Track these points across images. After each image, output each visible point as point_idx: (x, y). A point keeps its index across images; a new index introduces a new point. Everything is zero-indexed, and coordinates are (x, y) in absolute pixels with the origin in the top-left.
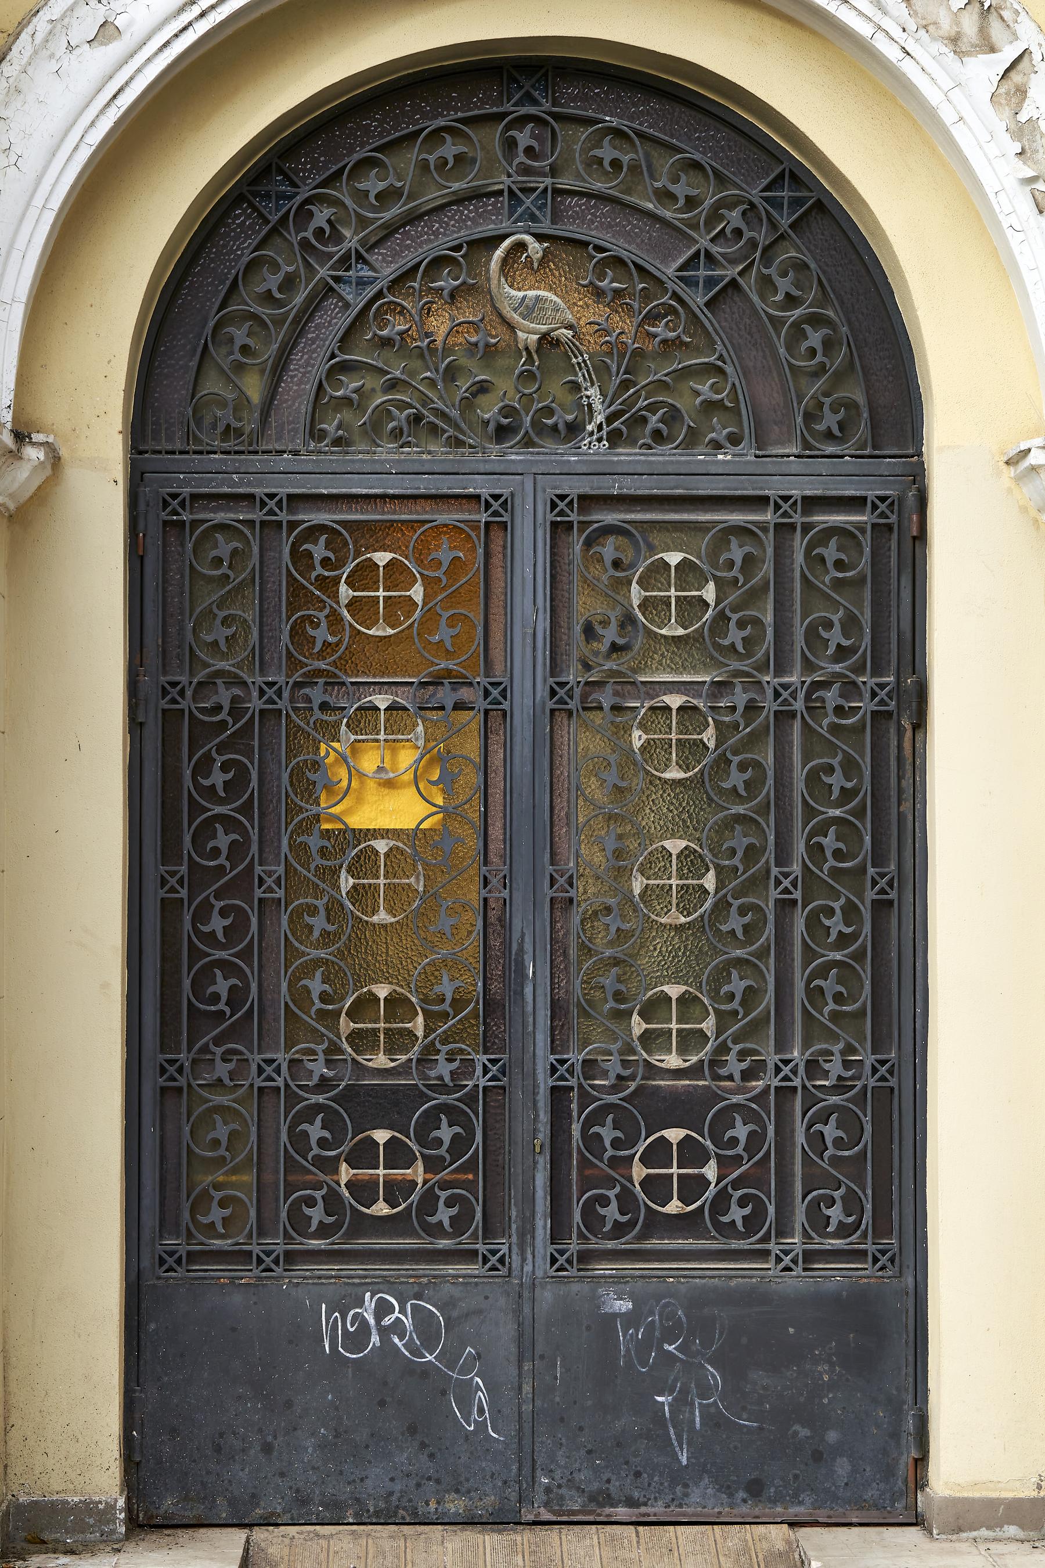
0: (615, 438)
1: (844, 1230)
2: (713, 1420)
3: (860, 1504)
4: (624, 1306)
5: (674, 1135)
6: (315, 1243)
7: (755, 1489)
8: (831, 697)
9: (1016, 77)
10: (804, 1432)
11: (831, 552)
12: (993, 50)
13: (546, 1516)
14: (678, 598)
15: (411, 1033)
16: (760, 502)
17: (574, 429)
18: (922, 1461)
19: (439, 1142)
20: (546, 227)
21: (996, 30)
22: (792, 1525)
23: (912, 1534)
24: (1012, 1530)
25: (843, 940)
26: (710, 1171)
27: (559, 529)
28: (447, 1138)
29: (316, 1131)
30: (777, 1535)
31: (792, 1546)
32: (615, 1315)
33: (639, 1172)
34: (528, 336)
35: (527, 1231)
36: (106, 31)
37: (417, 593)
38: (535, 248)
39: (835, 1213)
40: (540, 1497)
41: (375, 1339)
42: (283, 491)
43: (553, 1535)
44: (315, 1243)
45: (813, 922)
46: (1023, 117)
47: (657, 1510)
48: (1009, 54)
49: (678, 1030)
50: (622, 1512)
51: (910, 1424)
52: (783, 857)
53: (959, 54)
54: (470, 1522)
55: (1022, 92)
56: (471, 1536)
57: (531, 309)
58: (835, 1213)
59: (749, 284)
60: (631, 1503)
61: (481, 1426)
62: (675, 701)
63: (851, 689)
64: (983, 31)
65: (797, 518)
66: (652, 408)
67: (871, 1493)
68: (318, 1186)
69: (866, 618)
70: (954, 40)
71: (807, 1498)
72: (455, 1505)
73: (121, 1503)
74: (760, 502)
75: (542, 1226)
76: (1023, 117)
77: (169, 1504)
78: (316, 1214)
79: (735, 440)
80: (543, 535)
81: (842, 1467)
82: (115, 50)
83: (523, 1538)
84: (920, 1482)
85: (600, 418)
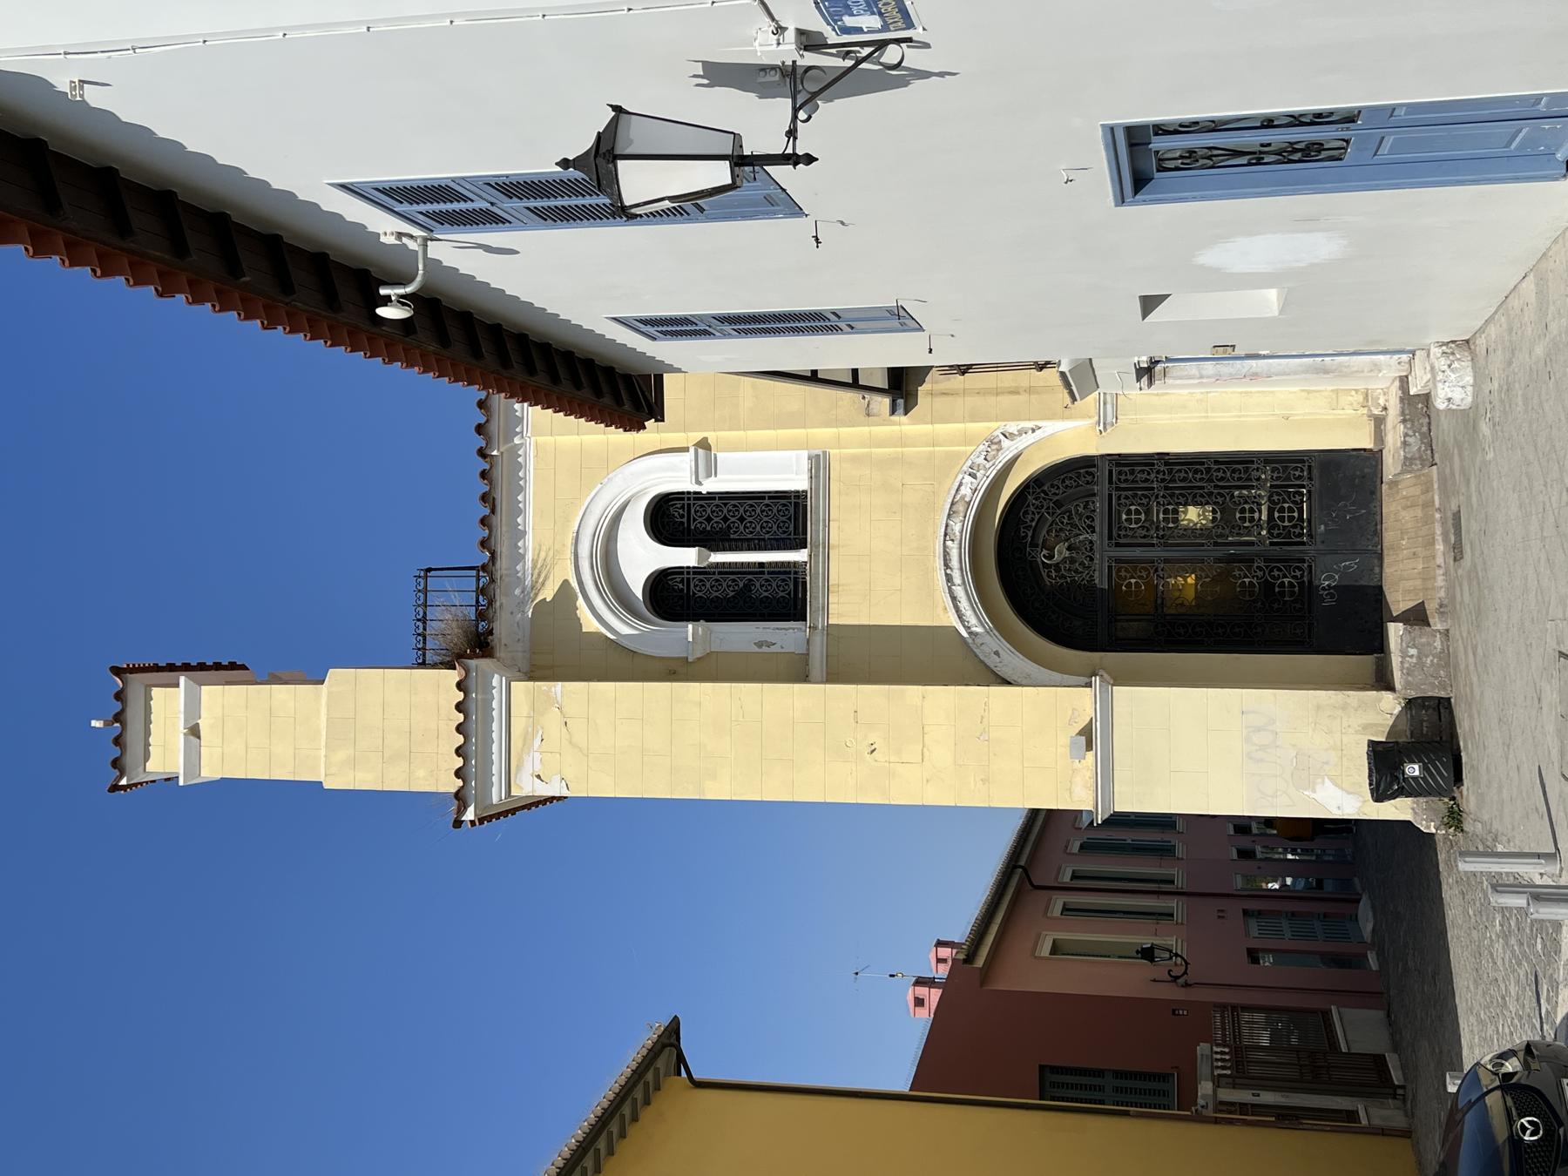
0: (1093, 532)
1: (1302, 471)
2: (1353, 504)
3: (1377, 466)
4: (1322, 527)
5: (1124, 517)
6: (1306, 606)
7: (1373, 493)
8: (1161, 476)
9: (1007, 435)
10: (1357, 480)
11: (1123, 477)
12: (1000, 441)
13: (1380, 547)
14: (1288, 516)
15: (1249, 582)
16: (1110, 496)
17: (1091, 542)
18: (1365, 450)
19: (1278, 575)
20: (1039, 549)
21: (996, 440)
22: (1382, 483)
23: (1384, 451)
24: (1382, 427)
25: (1224, 472)
26: (1286, 505)
27: (1118, 545)
28: (1278, 573)
29: (1276, 606)
30: (1384, 487)
31: (1387, 483)
32: (1325, 529)
33: (1286, 524)
34: (1067, 554)
35: (1301, 552)
36: (997, 653)
37: (1133, 581)
38: (1045, 552)
39: (1297, 473)
40: (1375, 548)
41: (1332, 591)
42: (1107, 486)
43: (1384, 545)
44: (1306, 606)
45: (1222, 479)
46: (1017, 433)
47: (1378, 518)
48: (1002, 437)
49: (1288, 512)
50: (1379, 527)
51: (1354, 453)
52: (1203, 488)
53: (1001, 449)
54: (1381, 566)
55: (1010, 434)
56: (1385, 565)
57: (1060, 553)
58: (1297, 473)
59: (1055, 499)
60: (1376, 525)
61: (1356, 564)
62: (1161, 516)
63: (1158, 472)
64: (996, 444)
65: (1114, 486)
66: (1085, 522)
67: (1374, 463)
68: (1290, 606)
69: (1140, 468)
70: (998, 450)
71: (1375, 479)
72: (1377, 570)
73: (1375, 655)
74: (1110, 496)
75: (1301, 548)
76: (1017, 433)
77: (1376, 644)
78: (1298, 606)
79: (1093, 502)
80: (1118, 549)
81: (1366, 470)
82: (1001, 652)
83: (1385, 552)
84: (1371, 450)
85: (1088, 536)
